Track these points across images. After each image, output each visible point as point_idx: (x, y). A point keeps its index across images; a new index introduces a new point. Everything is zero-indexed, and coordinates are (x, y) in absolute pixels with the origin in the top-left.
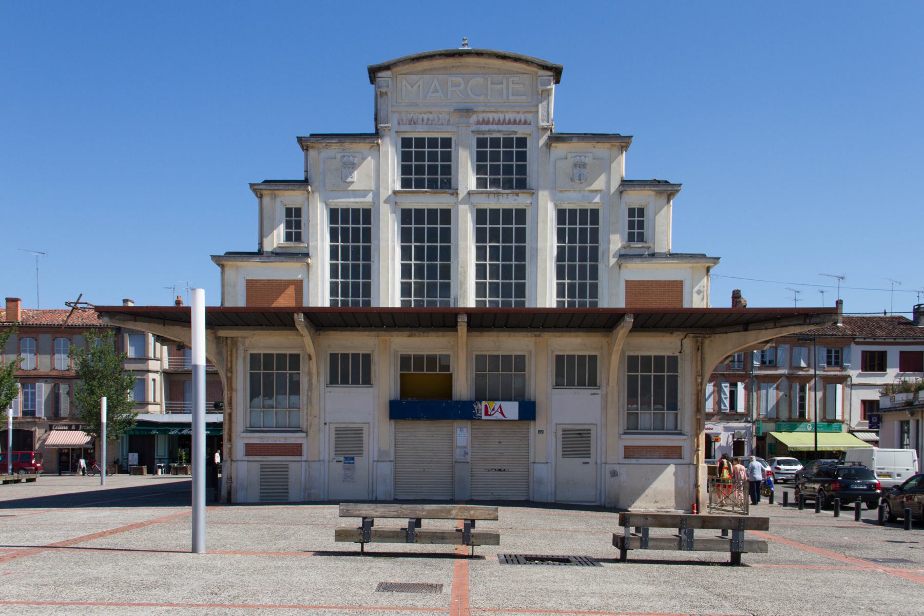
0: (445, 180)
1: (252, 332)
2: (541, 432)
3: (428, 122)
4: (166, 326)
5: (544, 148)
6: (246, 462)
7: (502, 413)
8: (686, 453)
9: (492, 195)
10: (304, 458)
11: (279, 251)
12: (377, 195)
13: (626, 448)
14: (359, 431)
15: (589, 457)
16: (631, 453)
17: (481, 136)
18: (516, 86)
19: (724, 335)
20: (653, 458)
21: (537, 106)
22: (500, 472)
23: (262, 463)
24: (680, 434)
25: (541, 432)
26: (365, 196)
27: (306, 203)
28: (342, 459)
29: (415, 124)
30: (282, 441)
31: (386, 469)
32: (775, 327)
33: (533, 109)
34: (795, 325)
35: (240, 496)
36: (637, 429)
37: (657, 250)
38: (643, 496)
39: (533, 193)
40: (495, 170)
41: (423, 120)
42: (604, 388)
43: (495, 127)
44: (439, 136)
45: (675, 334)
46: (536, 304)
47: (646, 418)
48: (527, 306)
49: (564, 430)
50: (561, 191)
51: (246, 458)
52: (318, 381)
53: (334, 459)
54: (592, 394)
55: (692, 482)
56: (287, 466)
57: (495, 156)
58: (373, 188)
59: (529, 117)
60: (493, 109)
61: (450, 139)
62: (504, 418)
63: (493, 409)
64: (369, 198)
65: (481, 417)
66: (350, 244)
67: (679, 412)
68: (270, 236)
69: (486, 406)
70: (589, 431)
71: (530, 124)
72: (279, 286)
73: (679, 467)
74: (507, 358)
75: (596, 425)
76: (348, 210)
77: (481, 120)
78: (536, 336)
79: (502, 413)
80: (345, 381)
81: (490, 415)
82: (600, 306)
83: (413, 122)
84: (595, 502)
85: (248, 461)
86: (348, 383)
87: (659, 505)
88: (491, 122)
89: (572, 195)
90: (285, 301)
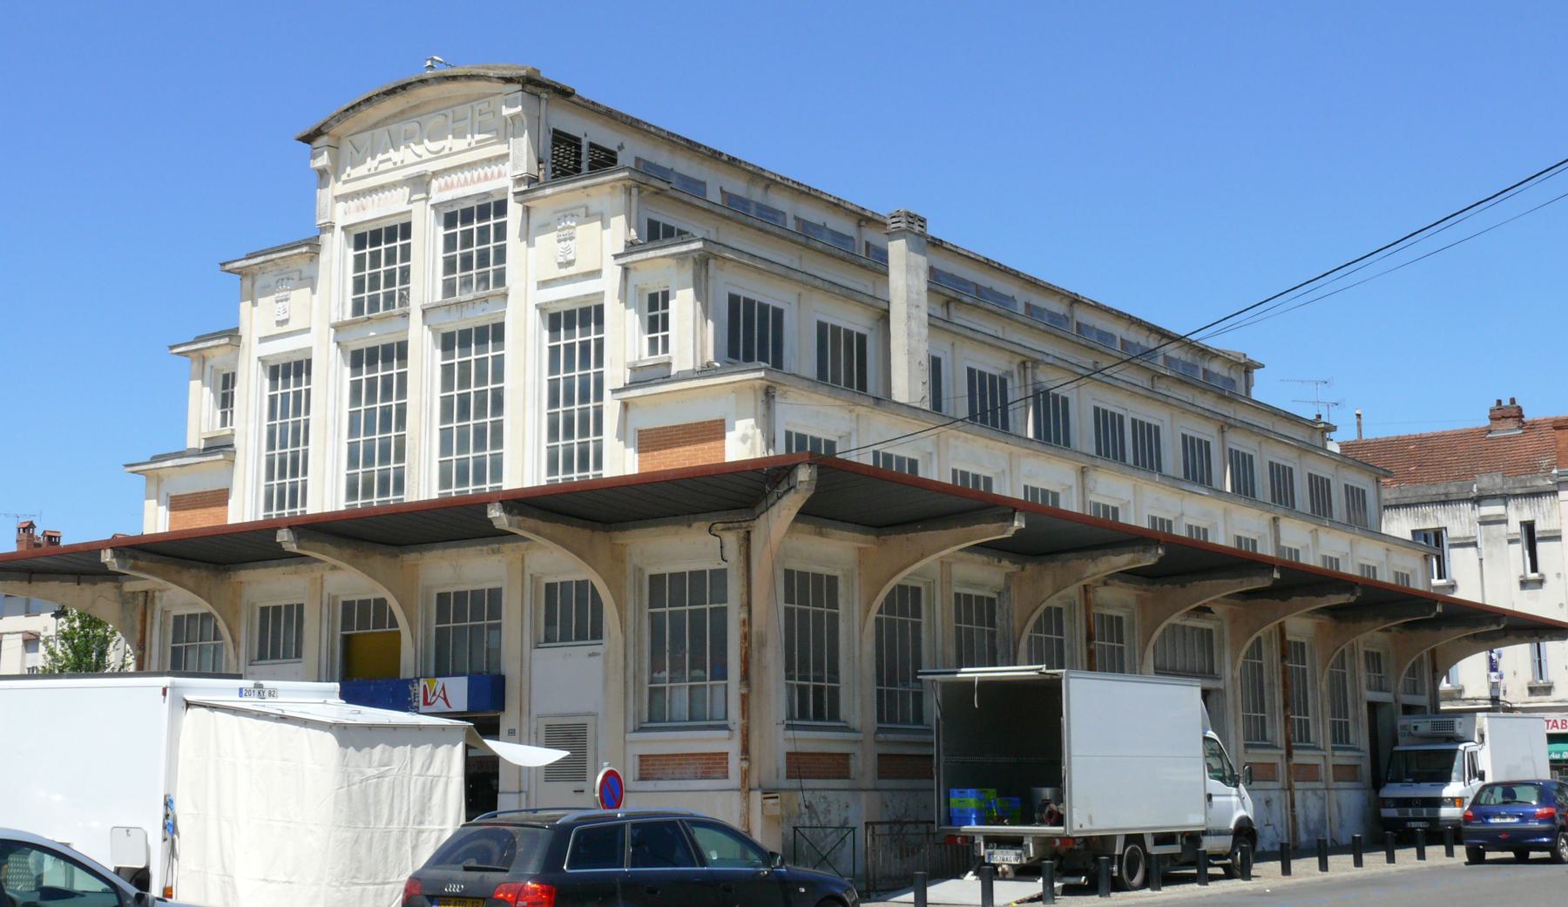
4: (33, 583)
7: (445, 699)
13: (643, 758)
20: (684, 779)
29: (364, 209)
45: (696, 525)
46: (227, 521)
47: (679, 698)
49: (548, 727)
52: (237, 657)
54: (590, 655)
63: (434, 694)
69: (425, 686)
79: (445, 699)
81: (430, 704)
88: (456, 185)
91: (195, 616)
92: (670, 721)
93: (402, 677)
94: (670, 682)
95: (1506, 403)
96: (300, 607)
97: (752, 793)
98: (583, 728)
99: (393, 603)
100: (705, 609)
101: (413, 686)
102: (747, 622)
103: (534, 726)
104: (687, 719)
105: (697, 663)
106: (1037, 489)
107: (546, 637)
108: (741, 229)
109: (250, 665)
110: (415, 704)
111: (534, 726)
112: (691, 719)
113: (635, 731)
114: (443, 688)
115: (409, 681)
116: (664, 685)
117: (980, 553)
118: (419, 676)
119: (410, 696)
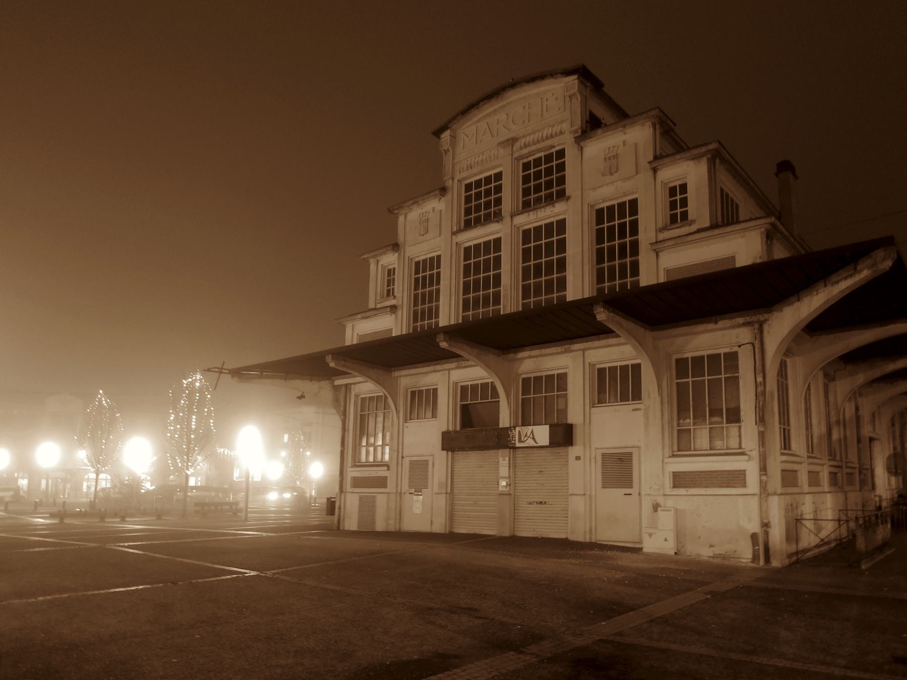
0: (498, 211)
2: (578, 458)
7: (534, 439)
19: (780, 341)
22: (541, 506)
24: (743, 454)
25: (578, 458)
28: (413, 491)
43: (533, 148)
49: (604, 455)
53: (408, 491)
54: (633, 410)
62: (537, 445)
65: (515, 444)
69: (519, 432)
70: (631, 454)
74: (550, 378)
79: (534, 439)
81: (523, 442)
91: (373, 397)
92: (695, 450)
93: (501, 426)
94: (693, 426)
96: (435, 390)
97: (770, 498)
98: (630, 455)
100: (688, 382)
101: (511, 431)
102: (762, 383)
103: (593, 456)
104: (709, 449)
107: (598, 401)
108: (477, 108)
109: (406, 422)
110: (513, 442)
111: (593, 456)
112: (711, 449)
113: (670, 457)
114: (532, 432)
115: (507, 429)
116: (690, 427)
118: (515, 425)
119: (510, 437)
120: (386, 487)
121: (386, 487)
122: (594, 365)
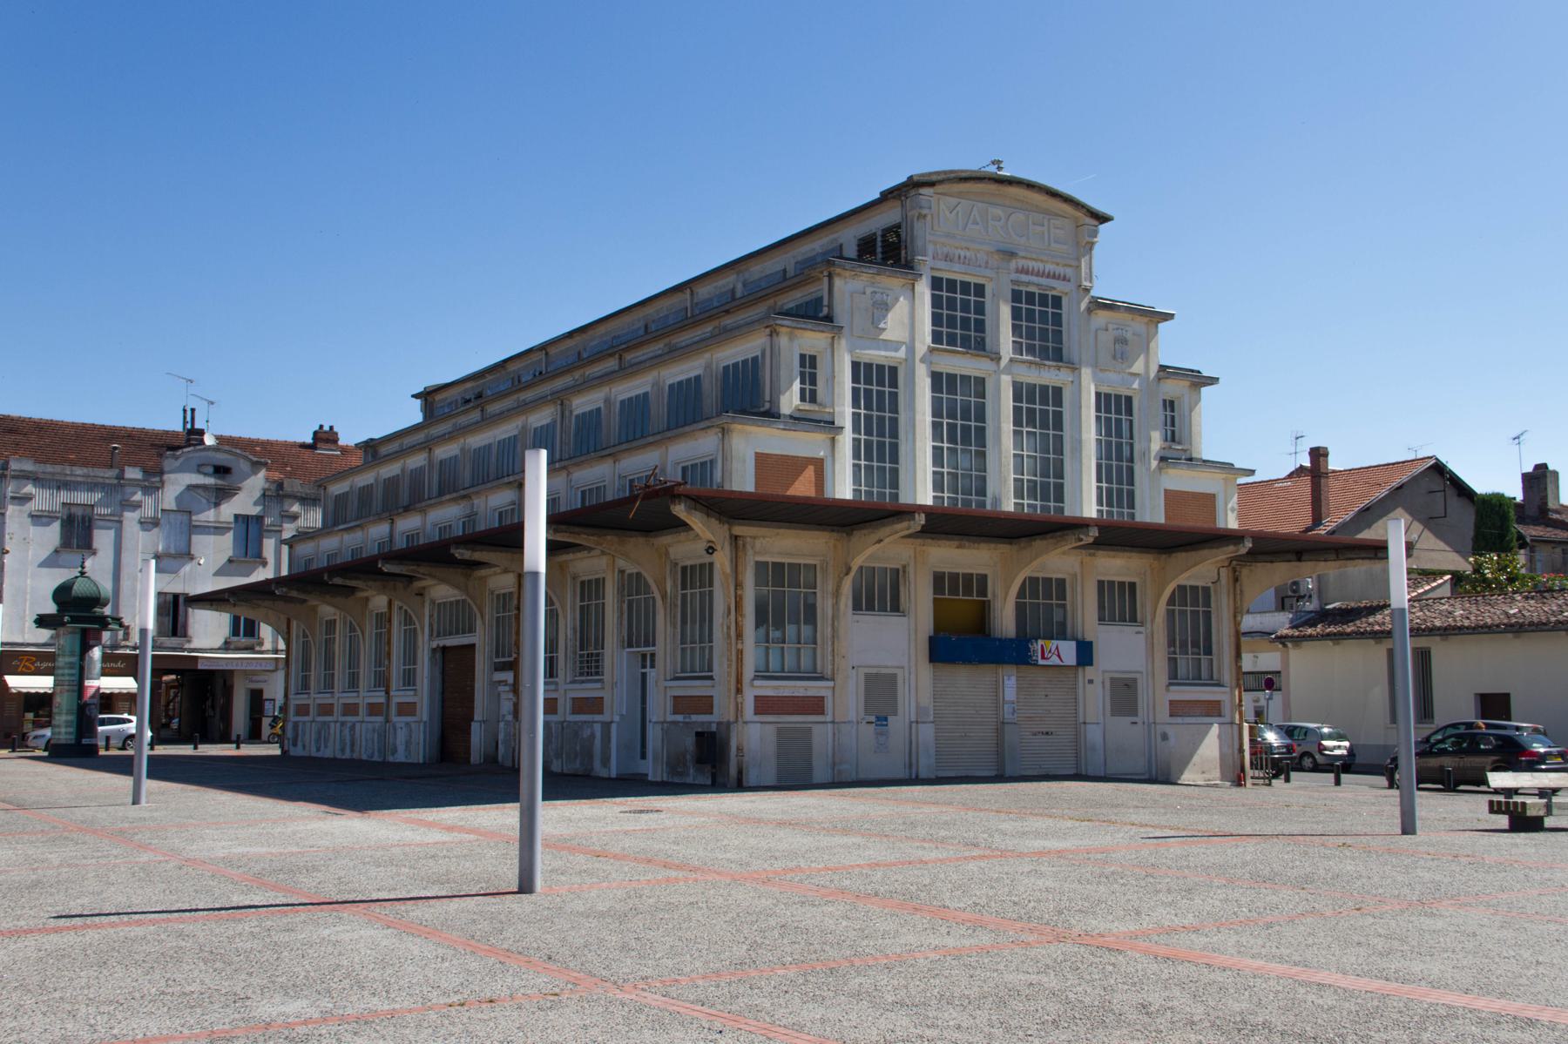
1: (776, 531)
2: (1091, 682)
3: (963, 261)
5: (1086, 313)
6: (759, 725)
7: (1059, 656)
8: (1226, 709)
9: (1033, 366)
10: (829, 718)
11: (797, 415)
12: (911, 350)
13: (1171, 702)
14: (892, 679)
15: (1136, 715)
16: (1177, 708)
17: (1016, 288)
18: (1058, 231)
19: (1269, 564)
21: (1079, 260)
23: (779, 725)
25: (1091, 682)
26: (896, 350)
27: (829, 350)
28: (873, 719)
30: (801, 693)
31: (927, 733)
32: (1338, 559)
33: (1074, 263)
34: (1363, 559)
35: (751, 777)
36: (1200, 679)
37: (1194, 455)
38: (1190, 766)
39: (1074, 368)
40: (1030, 335)
41: (959, 257)
42: (1149, 625)
44: (972, 280)
48: (1067, 513)
50: (1101, 370)
51: (757, 718)
53: (863, 719)
55: (1236, 746)
56: (810, 729)
57: (951, 304)
58: (907, 340)
59: (1069, 272)
60: (1034, 256)
61: (983, 286)
64: (902, 353)
66: (875, 413)
67: (1215, 658)
68: (788, 393)
69: (1042, 646)
71: (1069, 281)
72: (794, 465)
73: (1223, 726)
75: (903, 668)
76: (871, 365)
77: (1020, 267)
78: (1090, 555)
79: (1059, 656)
80: (870, 607)
82: (1138, 519)
83: (947, 258)
84: (1143, 774)
85: (762, 723)
86: (874, 610)
87: (1207, 776)
89: (1112, 376)
90: (802, 487)
95: (326, 428)
99: (469, 600)
105: (1195, 644)
106: (942, 374)
114: (1057, 648)
117: (910, 540)
120: (358, 715)
121: (358, 715)
122: (625, 477)
